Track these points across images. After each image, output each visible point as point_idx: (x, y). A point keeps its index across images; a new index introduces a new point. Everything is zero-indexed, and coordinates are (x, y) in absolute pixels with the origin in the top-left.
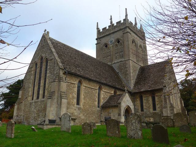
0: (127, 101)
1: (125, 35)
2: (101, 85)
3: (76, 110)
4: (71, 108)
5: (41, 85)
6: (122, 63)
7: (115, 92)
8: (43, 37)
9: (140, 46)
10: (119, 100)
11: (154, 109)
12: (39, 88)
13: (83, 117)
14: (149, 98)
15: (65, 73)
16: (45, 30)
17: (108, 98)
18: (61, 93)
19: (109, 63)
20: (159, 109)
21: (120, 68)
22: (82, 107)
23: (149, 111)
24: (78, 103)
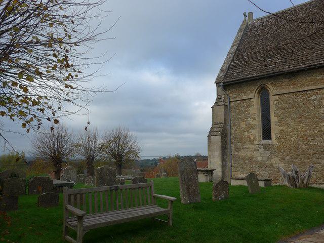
3: (258, 150)
24: (267, 134)
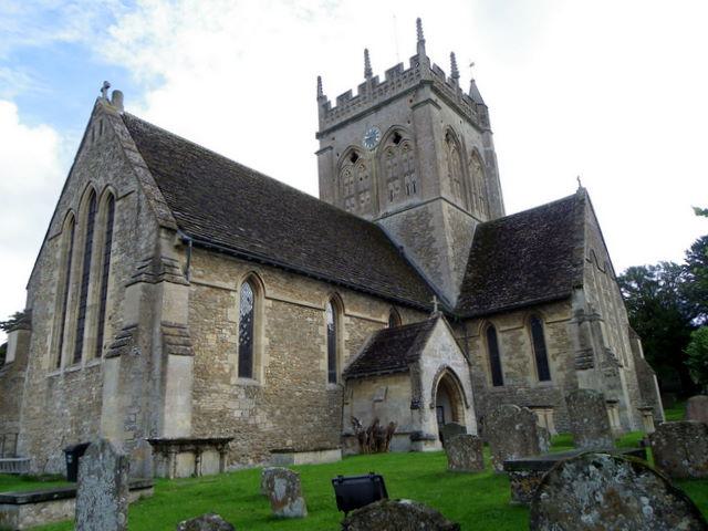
0: (444, 349)
1: (419, 111)
2: (339, 290)
3: (236, 396)
4: (216, 392)
5: (89, 302)
6: (412, 211)
7: (393, 318)
8: (98, 110)
9: (475, 153)
10: (410, 345)
11: (544, 374)
12: (82, 318)
13: (268, 426)
14: (521, 334)
15: (182, 247)
16: (107, 86)
17: (366, 342)
18: (165, 329)
19: (368, 217)
20: (561, 375)
21: (406, 227)
22: (263, 382)
23: (525, 385)
24: (246, 368)
